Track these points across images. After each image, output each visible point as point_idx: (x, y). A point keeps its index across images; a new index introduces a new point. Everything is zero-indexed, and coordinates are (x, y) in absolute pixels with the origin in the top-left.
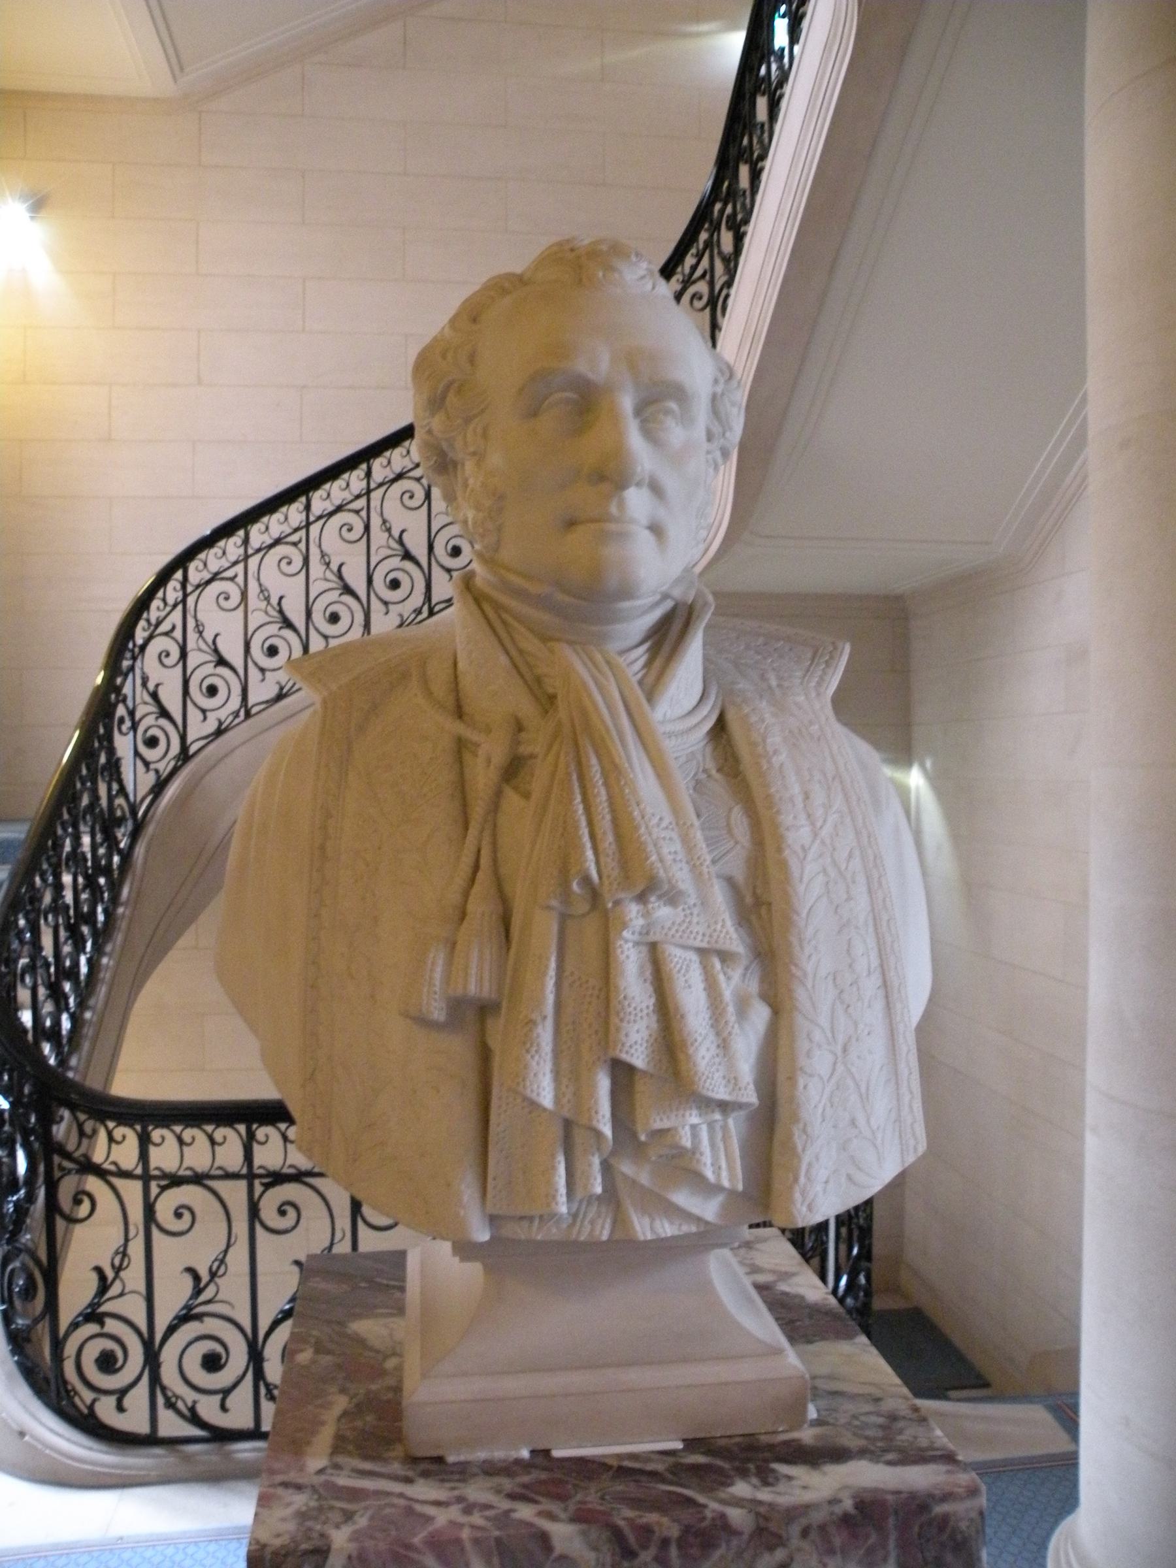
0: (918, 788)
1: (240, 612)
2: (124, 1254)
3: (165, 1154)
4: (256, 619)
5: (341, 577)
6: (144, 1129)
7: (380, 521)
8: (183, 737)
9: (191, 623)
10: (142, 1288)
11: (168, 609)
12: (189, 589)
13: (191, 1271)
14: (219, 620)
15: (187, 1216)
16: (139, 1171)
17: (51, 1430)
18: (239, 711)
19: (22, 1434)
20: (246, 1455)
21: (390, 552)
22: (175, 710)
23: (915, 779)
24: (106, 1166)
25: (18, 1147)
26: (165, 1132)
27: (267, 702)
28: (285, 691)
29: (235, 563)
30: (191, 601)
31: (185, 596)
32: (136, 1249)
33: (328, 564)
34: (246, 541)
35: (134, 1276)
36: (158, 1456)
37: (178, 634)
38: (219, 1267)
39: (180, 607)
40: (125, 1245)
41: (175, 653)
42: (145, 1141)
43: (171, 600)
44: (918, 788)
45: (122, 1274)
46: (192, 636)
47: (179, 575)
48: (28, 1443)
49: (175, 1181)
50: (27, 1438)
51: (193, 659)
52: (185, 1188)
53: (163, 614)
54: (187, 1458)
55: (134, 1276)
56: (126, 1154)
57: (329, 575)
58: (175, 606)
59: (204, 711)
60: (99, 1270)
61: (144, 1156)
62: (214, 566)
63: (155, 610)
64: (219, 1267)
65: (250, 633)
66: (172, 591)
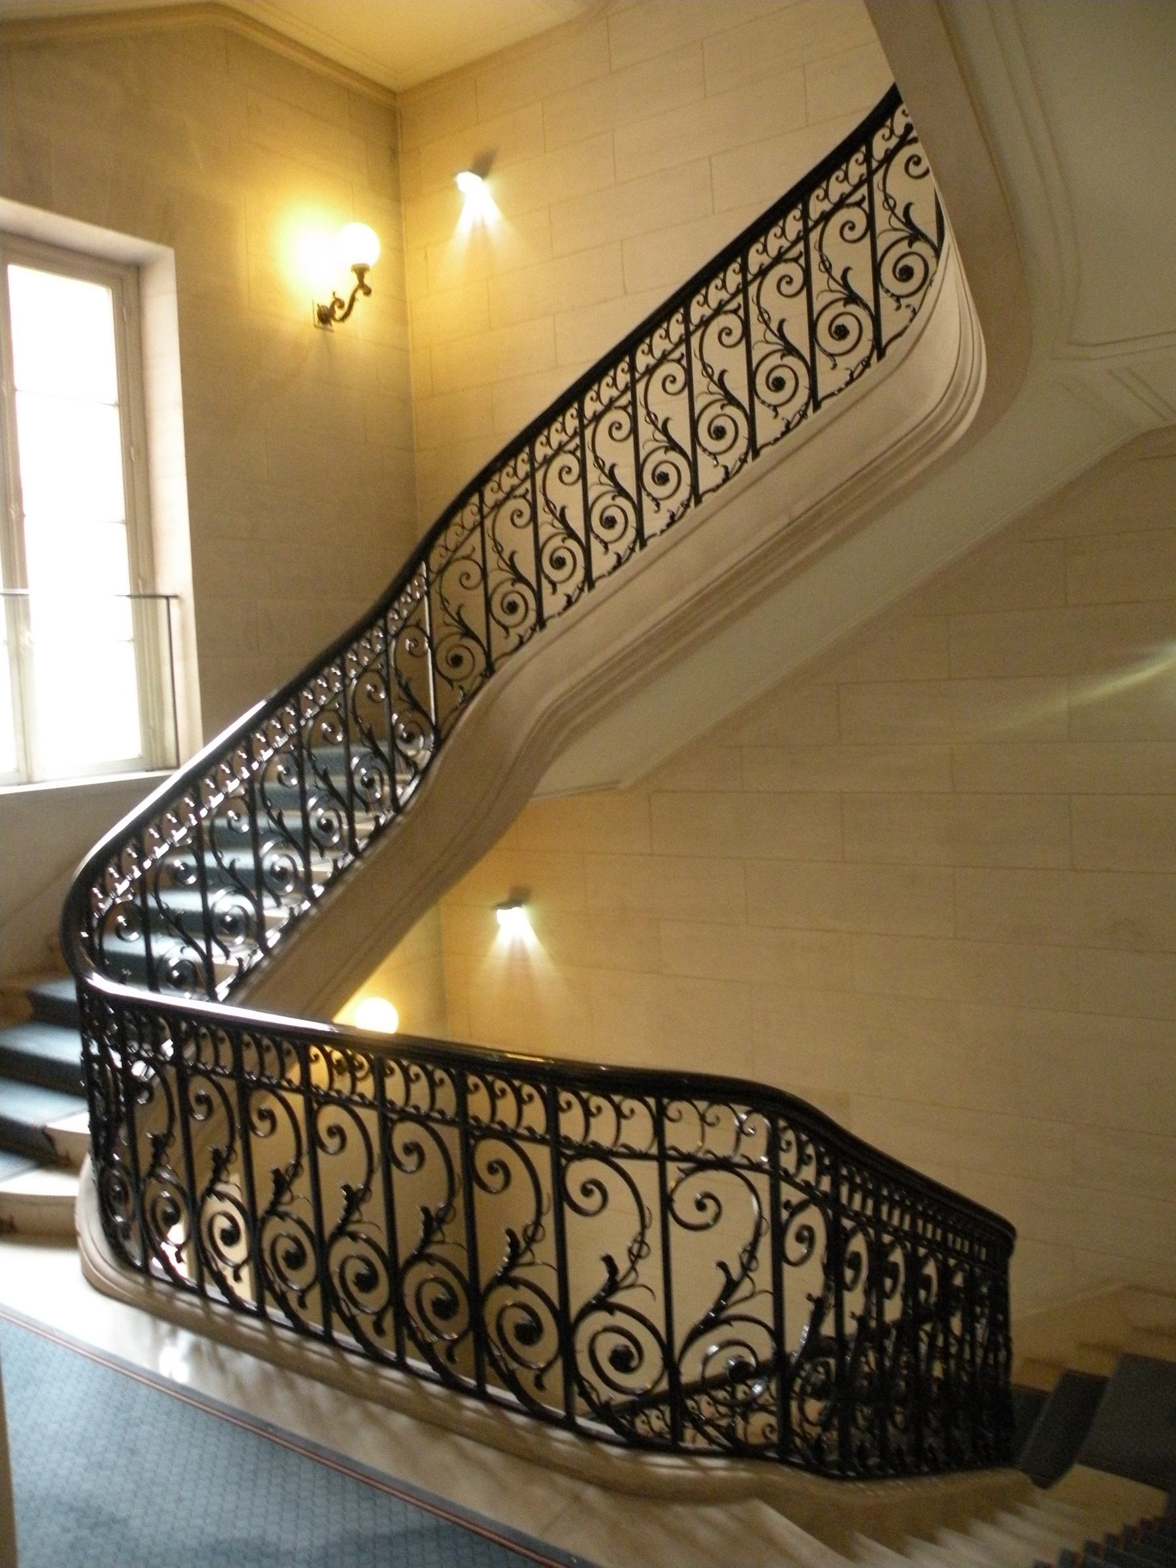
2: (642, 1243)
3: (684, 1132)
4: (545, 531)
6: (659, 1104)
8: (488, 654)
9: (489, 543)
10: (553, 1262)
11: (466, 532)
12: (486, 510)
13: (722, 1266)
15: (710, 1203)
16: (654, 1151)
20: (665, 1471)
21: (657, 445)
22: (479, 628)
24: (737, 1159)
25: (112, 1051)
26: (684, 1106)
30: (488, 523)
31: (483, 517)
32: (548, 1221)
33: (892, 209)
35: (545, 1250)
37: (478, 556)
38: (640, 1249)
39: (478, 531)
40: (642, 1234)
41: (476, 573)
42: (659, 1120)
43: (469, 524)
45: (535, 1247)
46: (492, 557)
47: (475, 499)
49: (700, 1164)
51: (494, 578)
52: (712, 1174)
53: (461, 539)
55: (545, 1250)
56: (638, 1131)
57: (770, 337)
58: (472, 530)
59: (506, 628)
60: (608, 1260)
61: (659, 1132)
63: (451, 536)
64: (640, 1249)
66: (469, 515)
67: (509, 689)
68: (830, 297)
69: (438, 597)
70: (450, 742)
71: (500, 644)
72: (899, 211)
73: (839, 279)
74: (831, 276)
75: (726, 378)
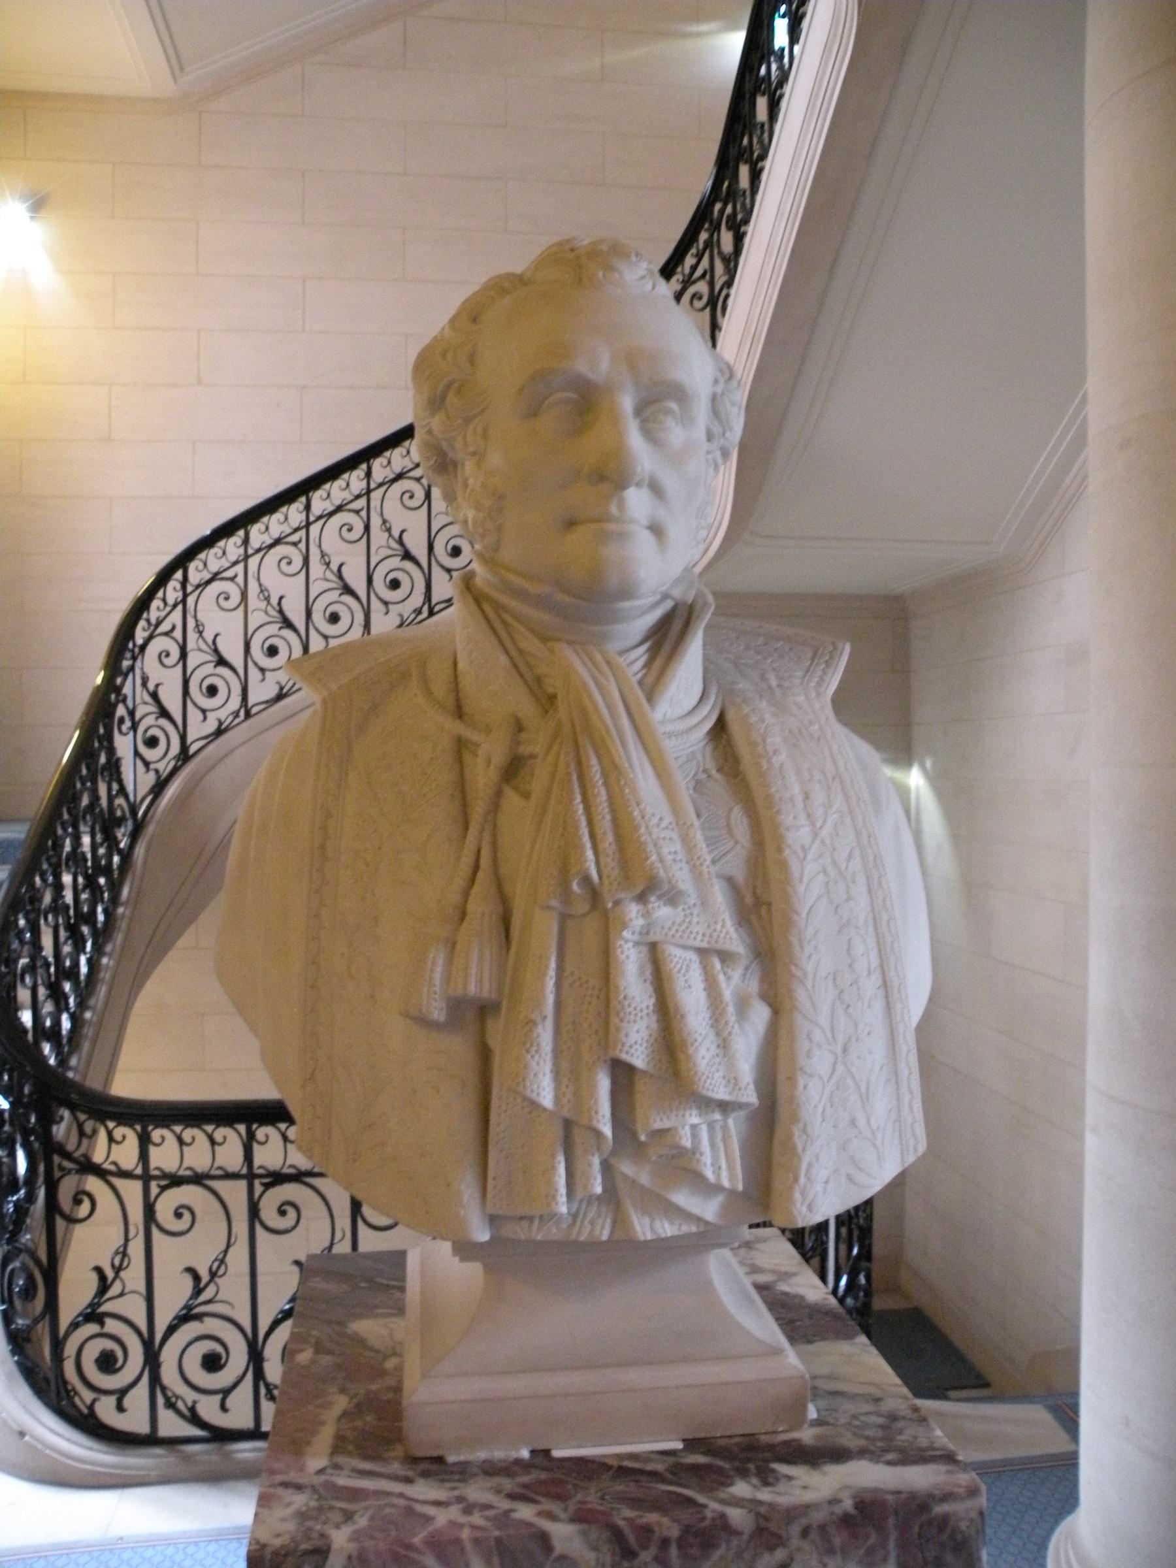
0: (918, 788)
1: (240, 612)
2: (124, 1254)
3: (165, 1154)
4: (256, 619)
5: (341, 577)
6: (144, 1129)
7: (380, 521)
8: (183, 737)
9: (191, 623)
11: (168, 609)
12: (189, 589)
13: (191, 1271)
14: (219, 620)
16: (139, 1171)
17: (51, 1430)
18: (239, 711)
19: (22, 1434)
21: (390, 552)
22: (175, 710)
23: (915, 779)
26: (165, 1132)
27: (267, 702)
28: (285, 691)
29: (235, 563)
30: (191, 601)
31: (185, 596)
33: (328, 564)
34: (246, 541)
36: (158, 1456)
37: (178, 634)
39: (180, 607)
40: (125, 1245)
41: (175, 653)
42: (145, 1141)
43: (171, 600)
44: (918, 788)
46: (192, 636)
47: (179, 575)
48: (28, 1443)
49: (175, 1181)
50: (27, 1438)
51: (193, 659)
52: (185, 1188)
53: (163, 614)
54: (187, 1458)
56: (126, 1154)
57: (329, 575)
58: (175, 606)
59: (204, 711)
60: (99, 1270)
61: (144, 1156)
62: (214, 566)
65: (250, 633)
66: (172, 591)
67: (208, 777)
68: (385, 552)
69: (318, 551)
70: (150, 830)
71: (197, 729)
72: (274, 601)
73: (210, 641)
74: (390, 535)
75: (344, 569)
